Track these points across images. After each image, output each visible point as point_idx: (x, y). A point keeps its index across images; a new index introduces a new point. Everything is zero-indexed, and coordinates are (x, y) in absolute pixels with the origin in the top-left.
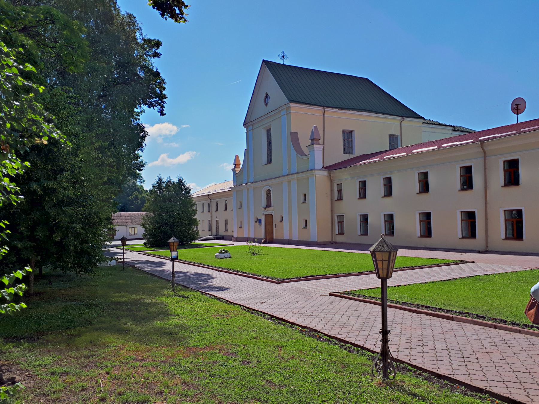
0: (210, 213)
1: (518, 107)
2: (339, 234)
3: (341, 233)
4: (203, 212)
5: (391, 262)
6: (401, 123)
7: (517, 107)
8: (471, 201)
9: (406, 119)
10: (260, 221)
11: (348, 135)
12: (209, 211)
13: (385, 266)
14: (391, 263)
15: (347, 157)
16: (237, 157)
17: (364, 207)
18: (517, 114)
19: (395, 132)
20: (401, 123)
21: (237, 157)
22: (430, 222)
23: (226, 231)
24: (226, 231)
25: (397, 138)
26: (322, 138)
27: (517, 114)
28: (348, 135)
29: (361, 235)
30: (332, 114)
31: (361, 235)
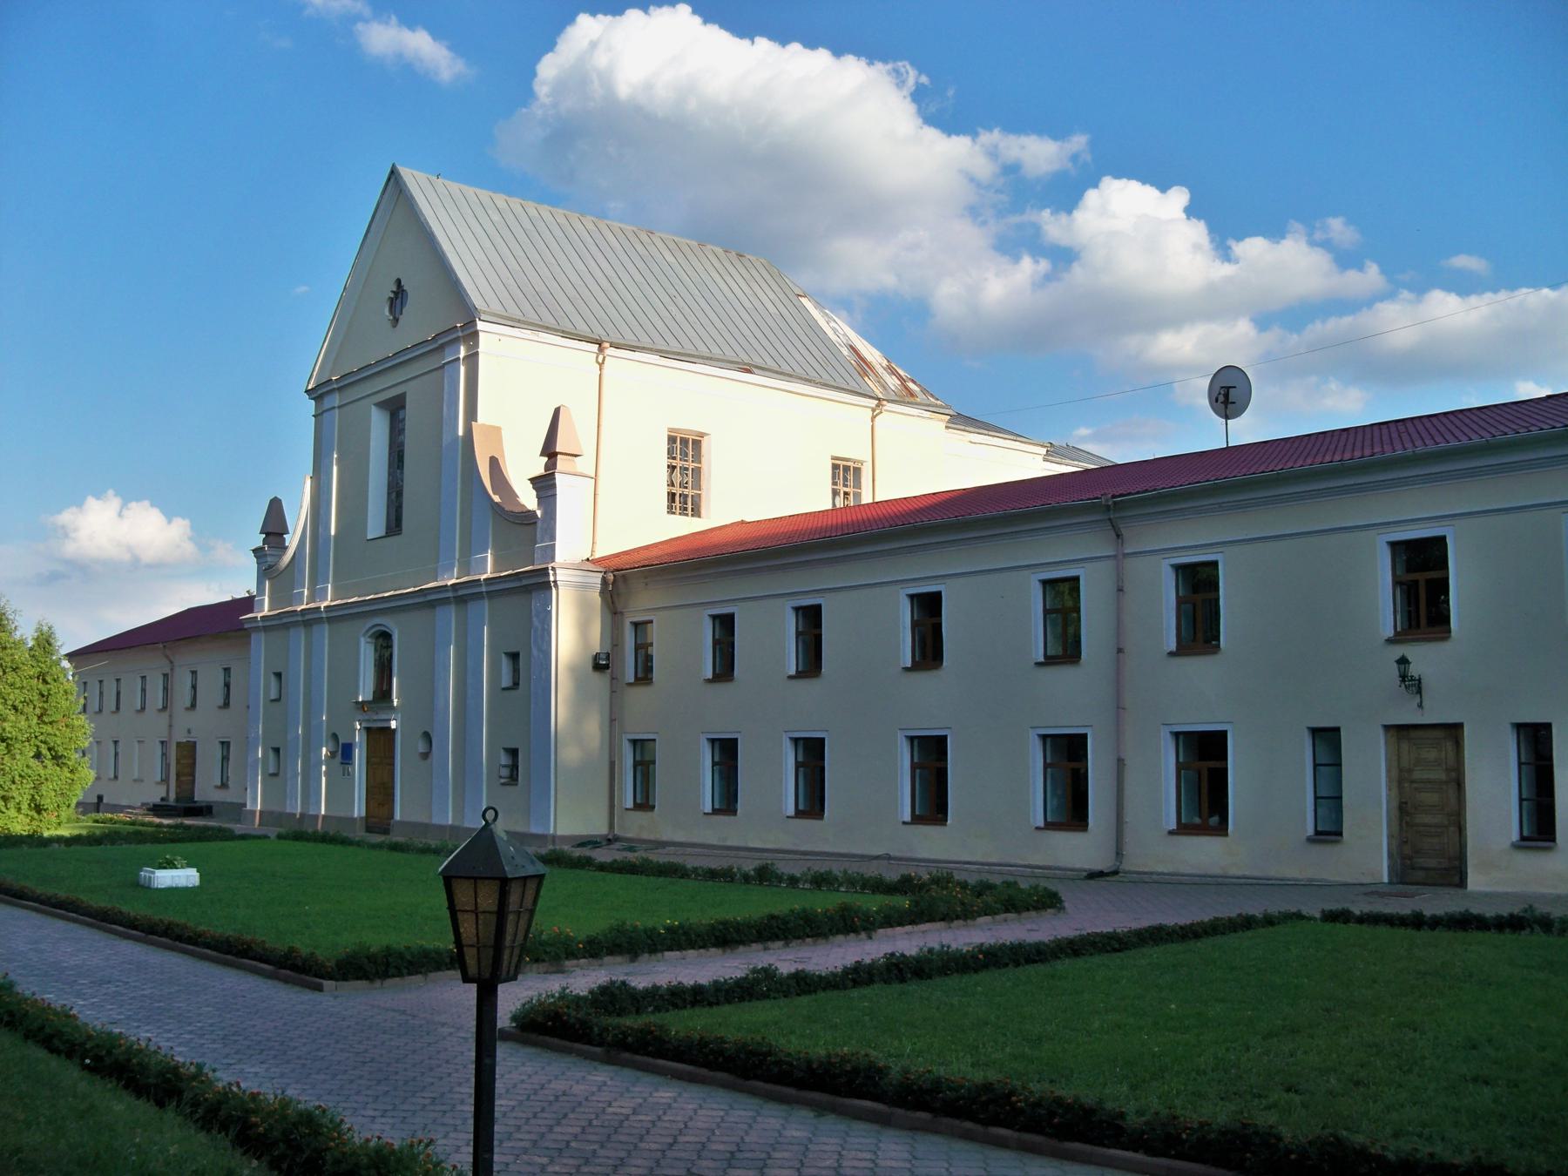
0: (166, 715)
1: (1228, 395)
2: (638, 807)
3: (644, 804)
4: (226, 704)
5: (511, 917)
6: (873, 418)
7: (1227, 396)
8: (1070, 701)
9: (889, 406)
10: (1143, 1115)
11: (685, 450)
12: (165, 708)
13: (488, 933)
14: (510, 929)
15: (684, 526)
16: (275, 507)
17: (724, 711)
18: (1227, 417)
19: (855, 450)
20: (873, 418)
21: (275, 507)
22: (1223, 773)
23: (224, 785)
24: (224, 785)
25: (857, 471)
26: (588, 451)
27: (1227, 417)
28: (685, 450)
29: (715, 812)
30: (629, 371)
31: (715, 812)
